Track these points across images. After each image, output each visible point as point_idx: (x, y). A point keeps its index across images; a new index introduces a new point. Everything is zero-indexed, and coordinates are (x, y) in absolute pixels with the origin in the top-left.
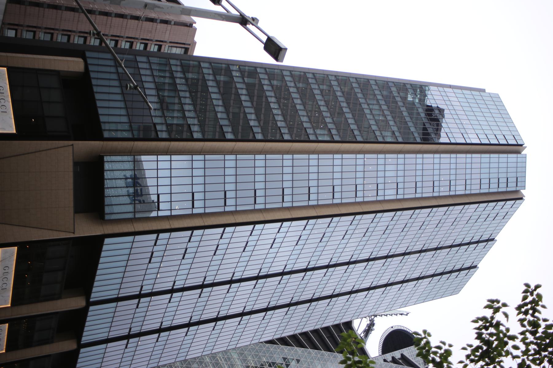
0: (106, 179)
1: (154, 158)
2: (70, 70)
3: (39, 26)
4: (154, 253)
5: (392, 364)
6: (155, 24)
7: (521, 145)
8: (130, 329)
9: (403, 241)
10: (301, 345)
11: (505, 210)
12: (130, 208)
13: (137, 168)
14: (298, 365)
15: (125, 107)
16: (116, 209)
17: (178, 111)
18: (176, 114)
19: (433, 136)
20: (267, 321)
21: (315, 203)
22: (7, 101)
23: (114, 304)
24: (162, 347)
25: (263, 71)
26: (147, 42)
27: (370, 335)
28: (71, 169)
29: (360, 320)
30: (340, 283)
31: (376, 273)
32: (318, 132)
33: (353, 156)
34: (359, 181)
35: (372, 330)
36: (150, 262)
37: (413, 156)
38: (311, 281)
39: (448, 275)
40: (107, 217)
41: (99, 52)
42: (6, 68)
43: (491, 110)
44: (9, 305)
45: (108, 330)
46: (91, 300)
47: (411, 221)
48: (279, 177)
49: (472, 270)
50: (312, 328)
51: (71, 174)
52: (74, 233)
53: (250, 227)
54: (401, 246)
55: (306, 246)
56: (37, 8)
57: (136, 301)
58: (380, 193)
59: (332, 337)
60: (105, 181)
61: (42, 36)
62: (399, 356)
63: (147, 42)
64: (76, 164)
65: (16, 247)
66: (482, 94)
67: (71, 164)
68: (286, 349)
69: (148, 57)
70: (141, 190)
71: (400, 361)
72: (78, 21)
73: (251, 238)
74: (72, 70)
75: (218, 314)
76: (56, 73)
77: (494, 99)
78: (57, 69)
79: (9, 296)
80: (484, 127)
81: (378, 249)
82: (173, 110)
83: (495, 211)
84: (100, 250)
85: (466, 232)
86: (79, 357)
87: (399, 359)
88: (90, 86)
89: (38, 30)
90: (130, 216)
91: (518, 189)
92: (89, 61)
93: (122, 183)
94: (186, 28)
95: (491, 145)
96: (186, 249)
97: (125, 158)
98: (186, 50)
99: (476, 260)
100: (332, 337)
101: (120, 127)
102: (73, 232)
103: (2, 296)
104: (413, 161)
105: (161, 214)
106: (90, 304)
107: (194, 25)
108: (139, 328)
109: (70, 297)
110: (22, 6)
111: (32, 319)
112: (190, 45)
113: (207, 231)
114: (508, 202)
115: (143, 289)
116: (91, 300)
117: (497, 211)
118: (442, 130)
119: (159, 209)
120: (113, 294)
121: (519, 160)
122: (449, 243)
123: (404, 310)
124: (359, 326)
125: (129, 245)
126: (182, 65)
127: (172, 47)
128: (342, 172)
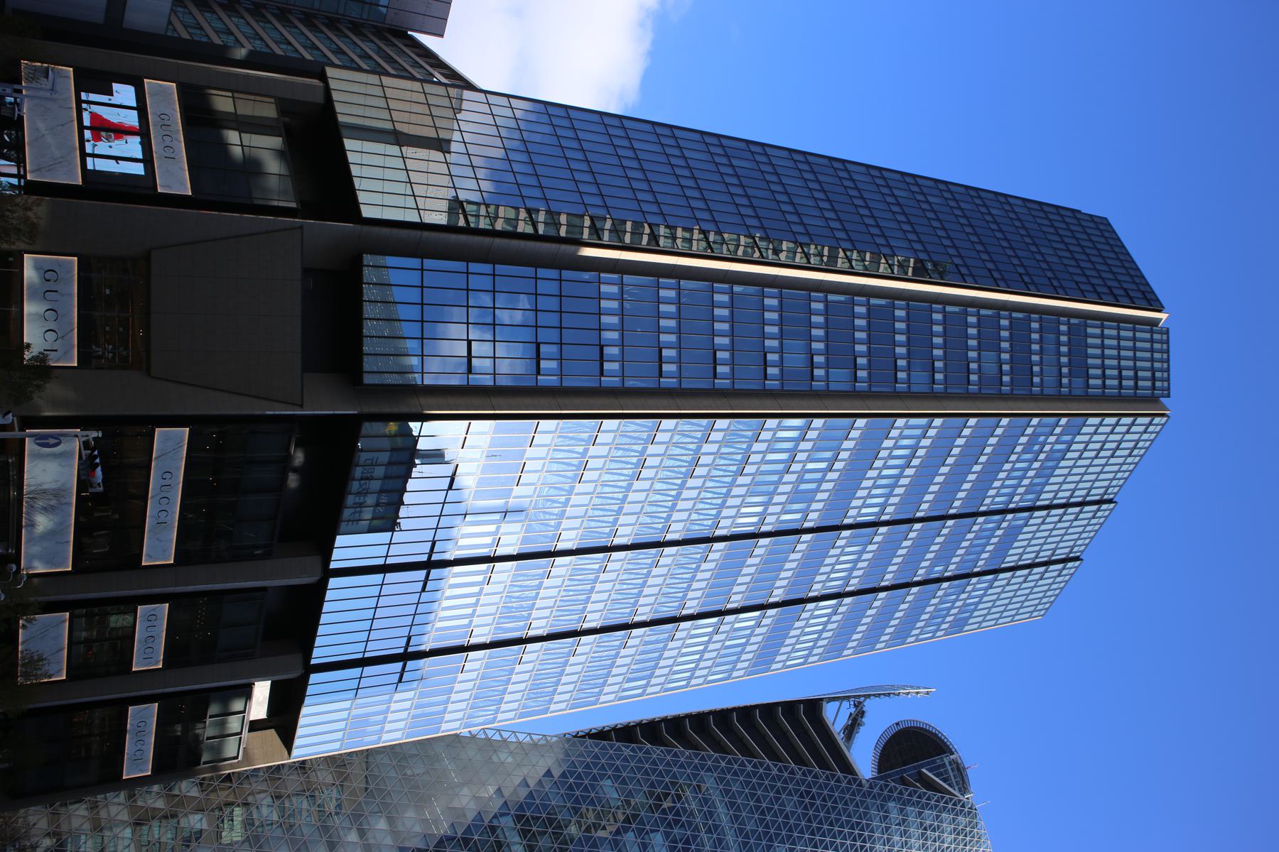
0: (366, 319)
27: (857, 735)
35: (859, 725)
36: (434, 543)
40: (368, 379)
46: (313, 662)
57: (398, 666)
60: (364, 322)
64: (306, 272)
79: (171, 541)
92: (333, 84)
102: (300, 403)
103: (158, 540)
116: (313, 662)
120: (353, 651)
124: (836, 717)
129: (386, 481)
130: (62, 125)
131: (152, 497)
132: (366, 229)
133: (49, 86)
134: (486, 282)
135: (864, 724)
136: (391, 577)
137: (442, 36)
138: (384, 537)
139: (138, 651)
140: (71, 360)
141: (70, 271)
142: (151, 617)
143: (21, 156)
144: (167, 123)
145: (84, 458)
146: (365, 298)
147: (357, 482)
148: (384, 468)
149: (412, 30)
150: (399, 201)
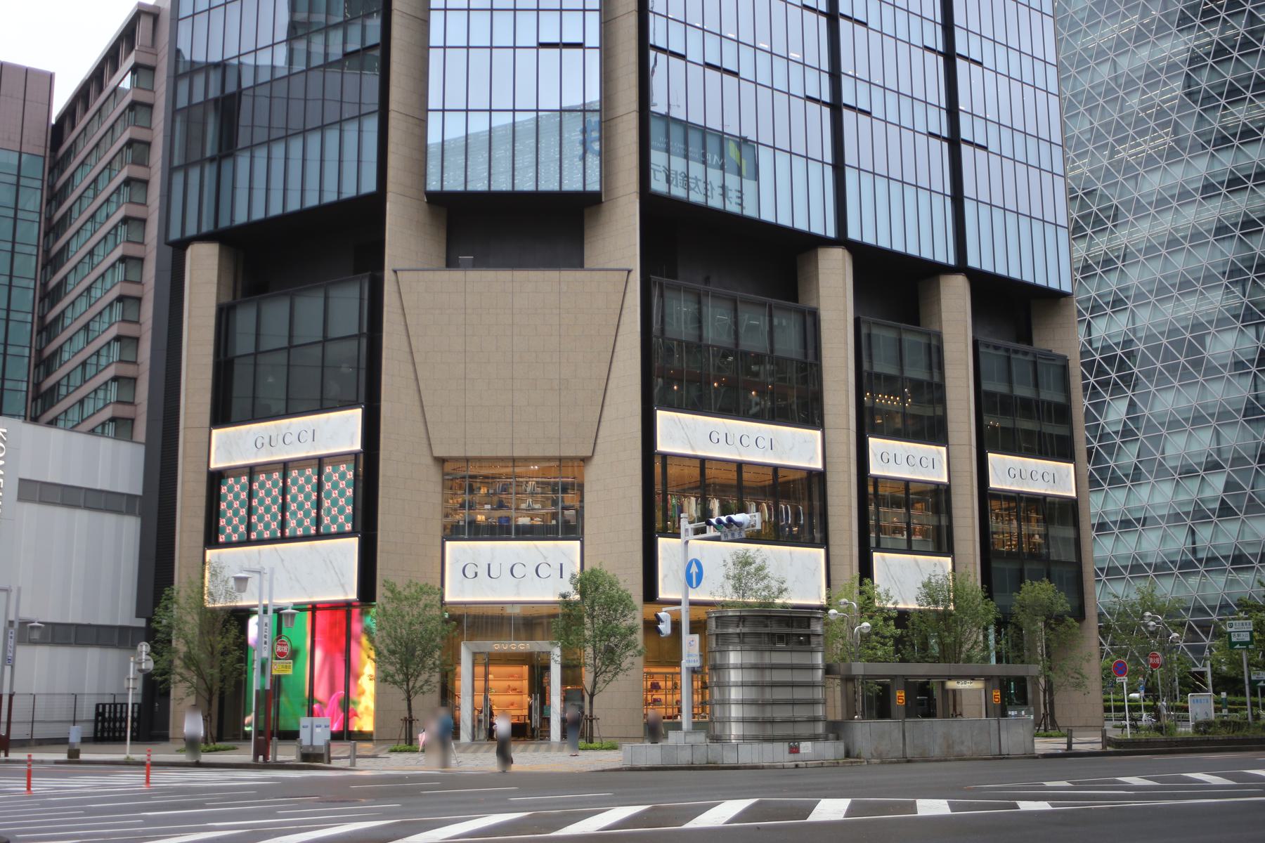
2: (215, 279)
4: (931, 130)
15: (302, 135)
22: (288, 428)
23: (969, 207)
36: (868, 113)
40: (593, 186)
44: (1072, 466)
45: (924, 196)
46: (952, 262)
52: (629, 271)
64: (451, 263)
65: (870, 439)
67: (457, 275)
74: (215, 273)
76: (225, 315)
86: (991, 270)
88: (251, 227)
92: (191, 230)
106: (961, 266)
109: (939, 300)
111: (983, 402)
116: (952, 262)
120: (942, 209)
125: (984, 210)
129: (709, 162)
130: (282, 560)
131: (740, 455)
133: (257, 576)
136: (850, 158)
137: (51, 77)
138: (765, 156)
139: (923, 475)
143: (944, 522)
144: (267, 440)
145: (718, 534)
147: (691, 193)
148: (709, 170)
150: (262, 119)
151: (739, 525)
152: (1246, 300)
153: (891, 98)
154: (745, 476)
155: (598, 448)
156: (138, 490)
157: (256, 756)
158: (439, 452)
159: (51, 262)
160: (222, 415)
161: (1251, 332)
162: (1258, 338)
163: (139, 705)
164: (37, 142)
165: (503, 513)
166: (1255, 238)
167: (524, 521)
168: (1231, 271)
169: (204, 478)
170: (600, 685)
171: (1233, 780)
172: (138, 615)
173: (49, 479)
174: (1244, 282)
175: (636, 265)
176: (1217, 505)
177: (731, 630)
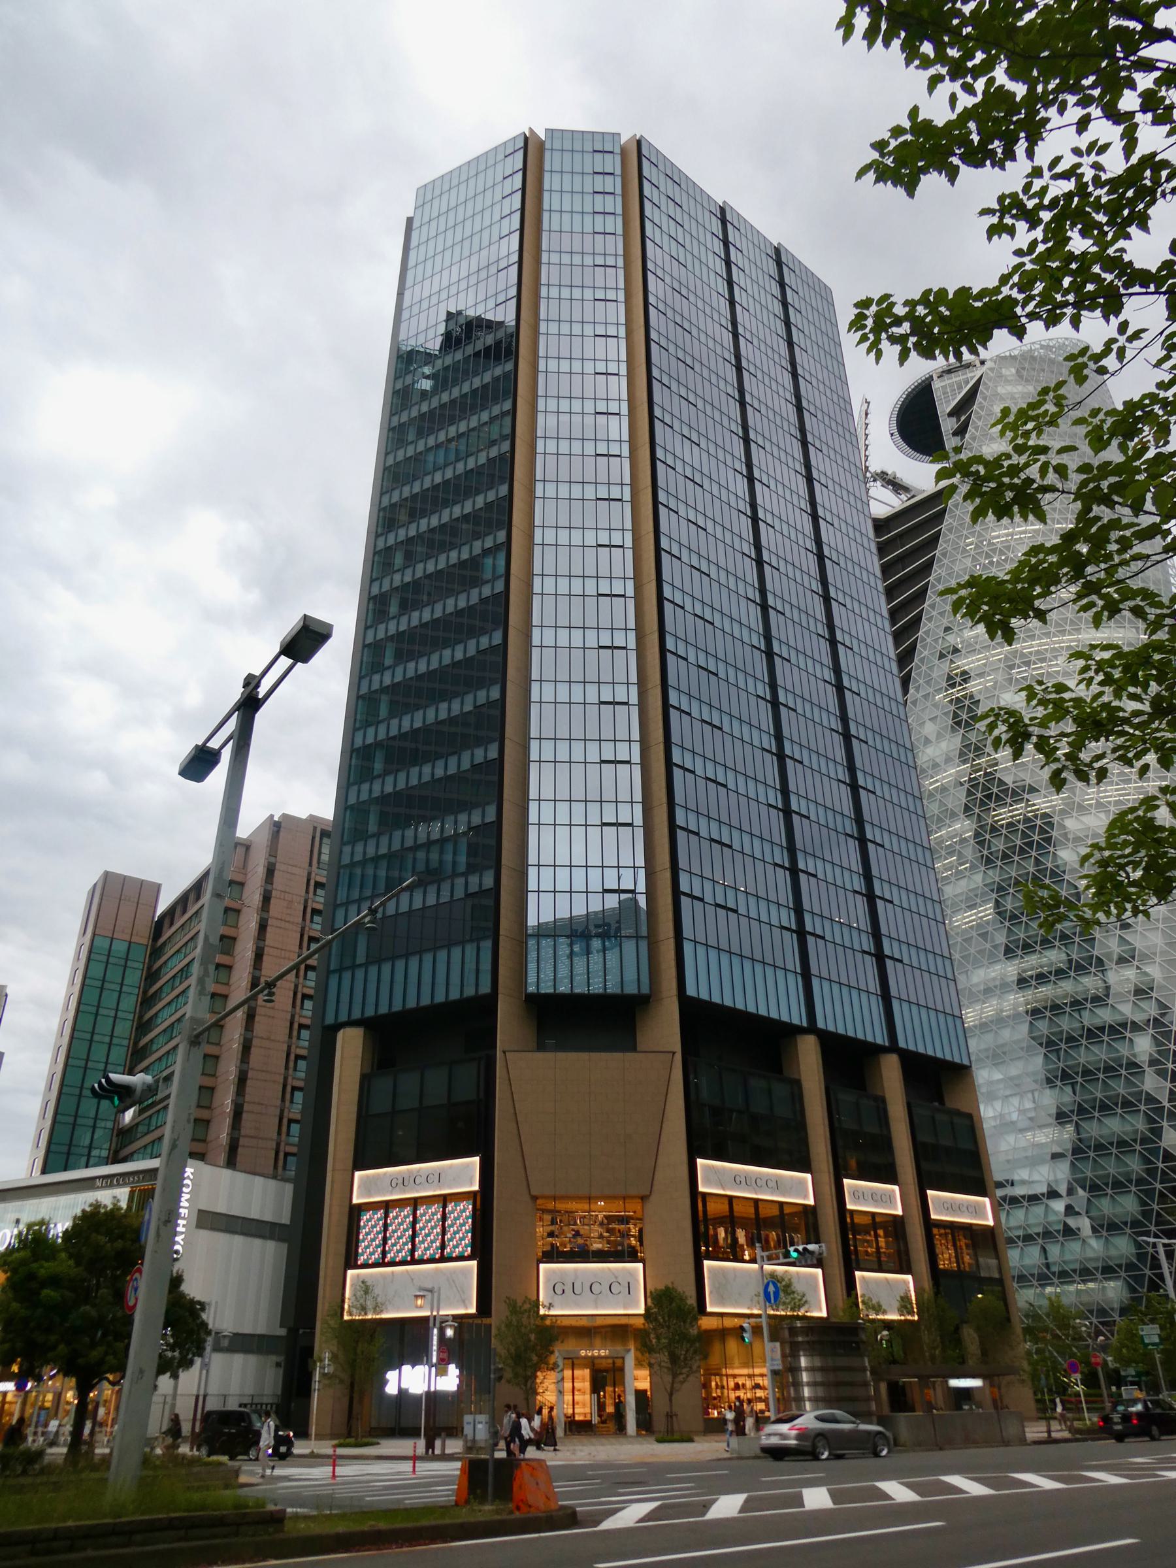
1: (532, 898)
3: (274, 1146)
5: (967, 436)
6: (274, 893)
7: (526, 139)
8: (864, 952)
9: (713, 367)
10: (916, 622)
11: (662, 182)
12: (629, 947)
13: (550, 931)
14: (955, 629)
16: (630, 974)
17: (441, 852)
18: (448, 857)
19: (501, 334)
20: (862, 686)
21: (630, 585)
24: (903, 893)
25: (365, 683)
26: (309, 910)
28: (549, 1055)
29: (872, 502)
30: (793, 537)
31: (777, 462)
32: (488, 575)
33: (538, 504)
34: (590, 492)
36: (702, 900)
37: (541, 378)
38: (786, 598)
39: (794, 330)
40: (645, 990)
41: (325, 1002)
42: (357, 1174)
43: (450, 251)
45: (864, 996)
46: (805, 1024)
47: (672, 348)
48: (577, 655)
49: (784, 259)
50: (883, 599)
51: (561, 1055)
52: (674, 1053)
53: (677, 773)
54: (721, 373)
55: (717, 605)
56: (245, 1116)
57: (810, 940)
58: (614, 450)
59: (902, 560)
61: (295, 1111)
62: (954, 419)
63: (309, 910)
64: (541, 1047)
66: (416, 224)
67: (540, 1055)
68: (922, 652)
69: (336, 906)
70: (597, 926)
71: (963, 418)
72: (268, 1039)
73: (699, 771)
75: (844, 783)
76: (366, 1081)
77: (429, 197)
78: (358, 1079)
80: (487, 223)
81: (729, 457)
82: (441, 862)
83: (662, 182)
84: (709, 1006)
85: (704, 269)
87: (958, 420)
89: (286, 1114)
90: (644, 945)
91: (617, 150)
92: (343, 1018)
93: (580, 964)
94: (281, 834)
95: (524, 189)
96: (712, 840)
97: (532, 956)
98: (325, 834)
99: (762, 247)
100: (902, 560)
101: (470, 965)
104: (553, 340)
105: (641, 887)
106: (812, 1028)
107: (276, 819)
108: (864, 937)
109: (798, 1057)
110: (241, 1143)
112: (315, 828)
113: (679, 798)
114: (646, 173)
115: (768, 747)
116: (805, 1024)
117: (664, 198)
118: (489, 316)
119: (633, 892)
121: (557, 145)
122: (724, 306)
123: (857, 408)
124: (884, 503)
125: (701, 950)
126: (353, 843)
127: (319, 862)
128: (587, 866)
132: (501, 989)
134: (547, 873)
135: (894, 473)
137: (159, 886)
140: (636, 1269)
141: (553, 1271)
142: (858, 1195)
144: (400, 1181)
146: (552, 991)
149: (153, 917)
151: (812, 1253)
152: (1061, 1065)
153: (763, 904)
154: (735, 1207)
155: (655, 1188)
156: (285, 1219)
157: (427, 1452)
158: (534, 1193)
159: (143, 1027)
160: (361, 1162)
161: (1069, 1089)
162: (1074, 1093)
163: (278, 1406)
164: (143, 935)
165: (580, 1241)
166: (1061, 1017)
167: (597, 1246)
168: (1047, 1043)
169: (347, 1209)
170: (677, 1386)
171: (1086, 1477)
172: (281, 1326)
173: (218, 1210)
174: (1058, 1051)
175: (677, 1047)
176: (1061, 1227)
177: (800, 1339)
